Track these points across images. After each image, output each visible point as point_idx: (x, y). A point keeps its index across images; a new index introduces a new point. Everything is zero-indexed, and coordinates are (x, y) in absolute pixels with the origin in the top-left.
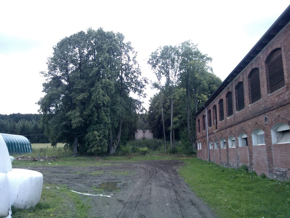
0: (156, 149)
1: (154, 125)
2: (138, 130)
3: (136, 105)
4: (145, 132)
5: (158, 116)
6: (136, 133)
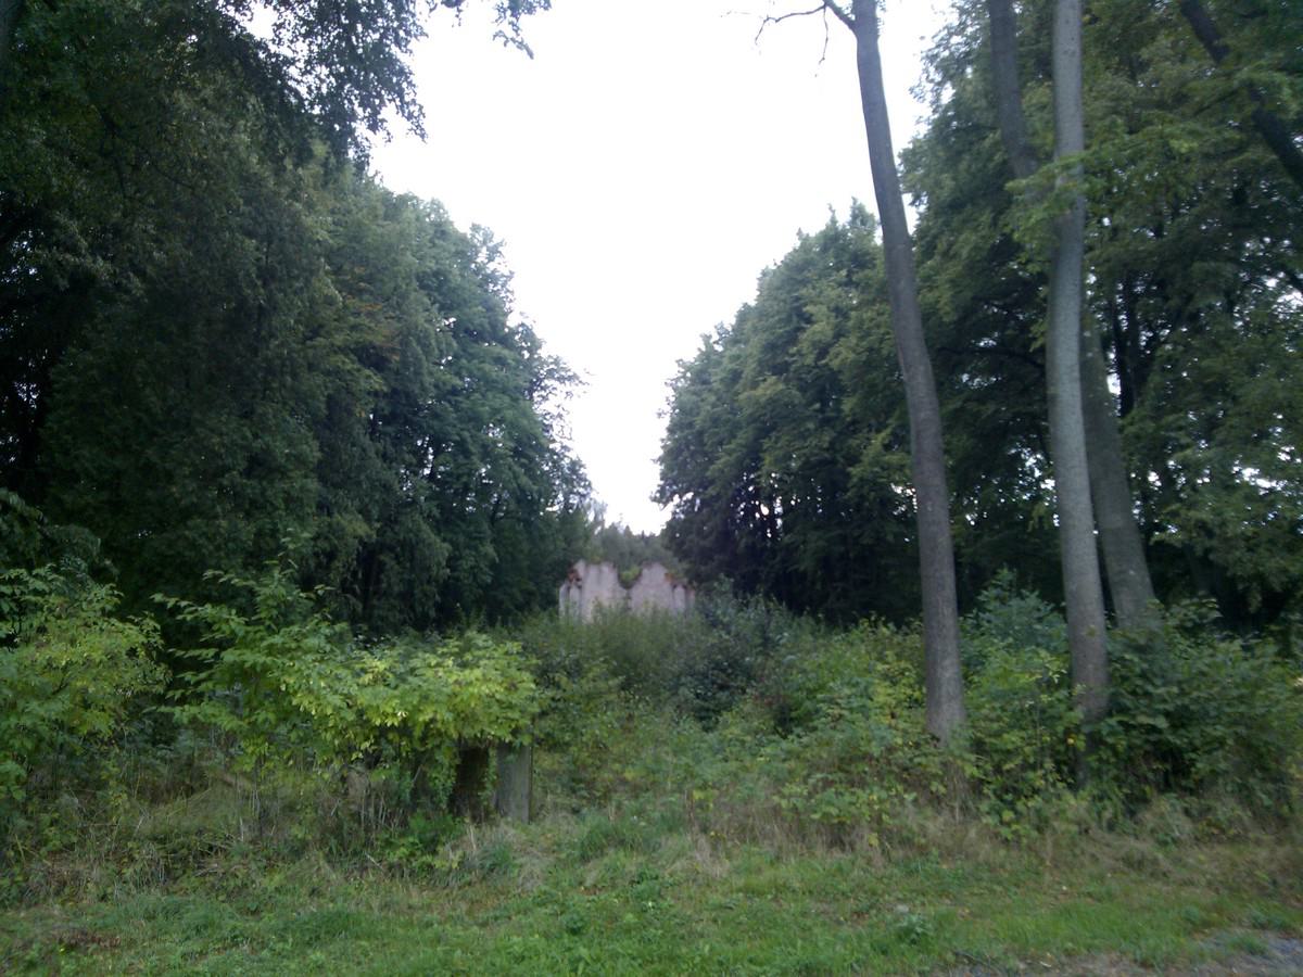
0: (728, 707)
1: (705, 538)
2: (580, 567)
3: (996, 334)
4: (638, 577)
5: (732, 459)
6: (569, 589)
